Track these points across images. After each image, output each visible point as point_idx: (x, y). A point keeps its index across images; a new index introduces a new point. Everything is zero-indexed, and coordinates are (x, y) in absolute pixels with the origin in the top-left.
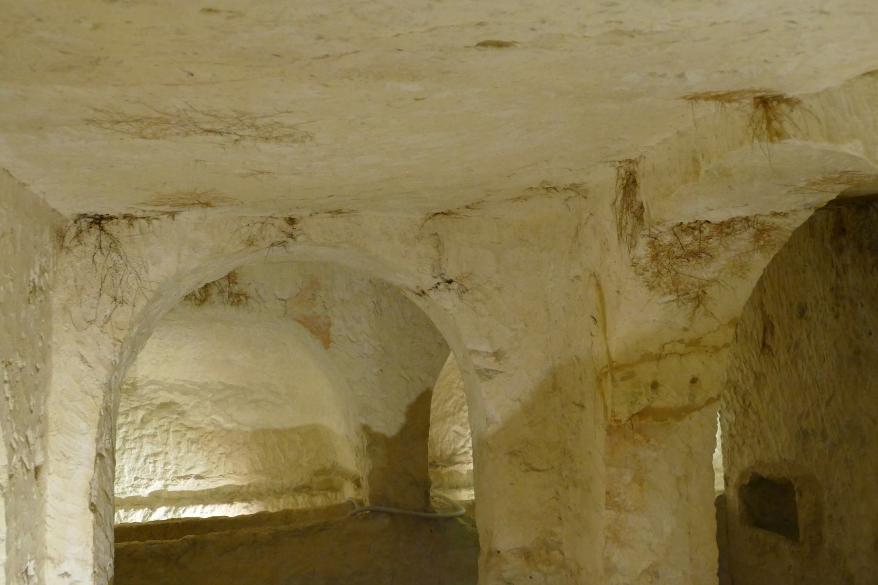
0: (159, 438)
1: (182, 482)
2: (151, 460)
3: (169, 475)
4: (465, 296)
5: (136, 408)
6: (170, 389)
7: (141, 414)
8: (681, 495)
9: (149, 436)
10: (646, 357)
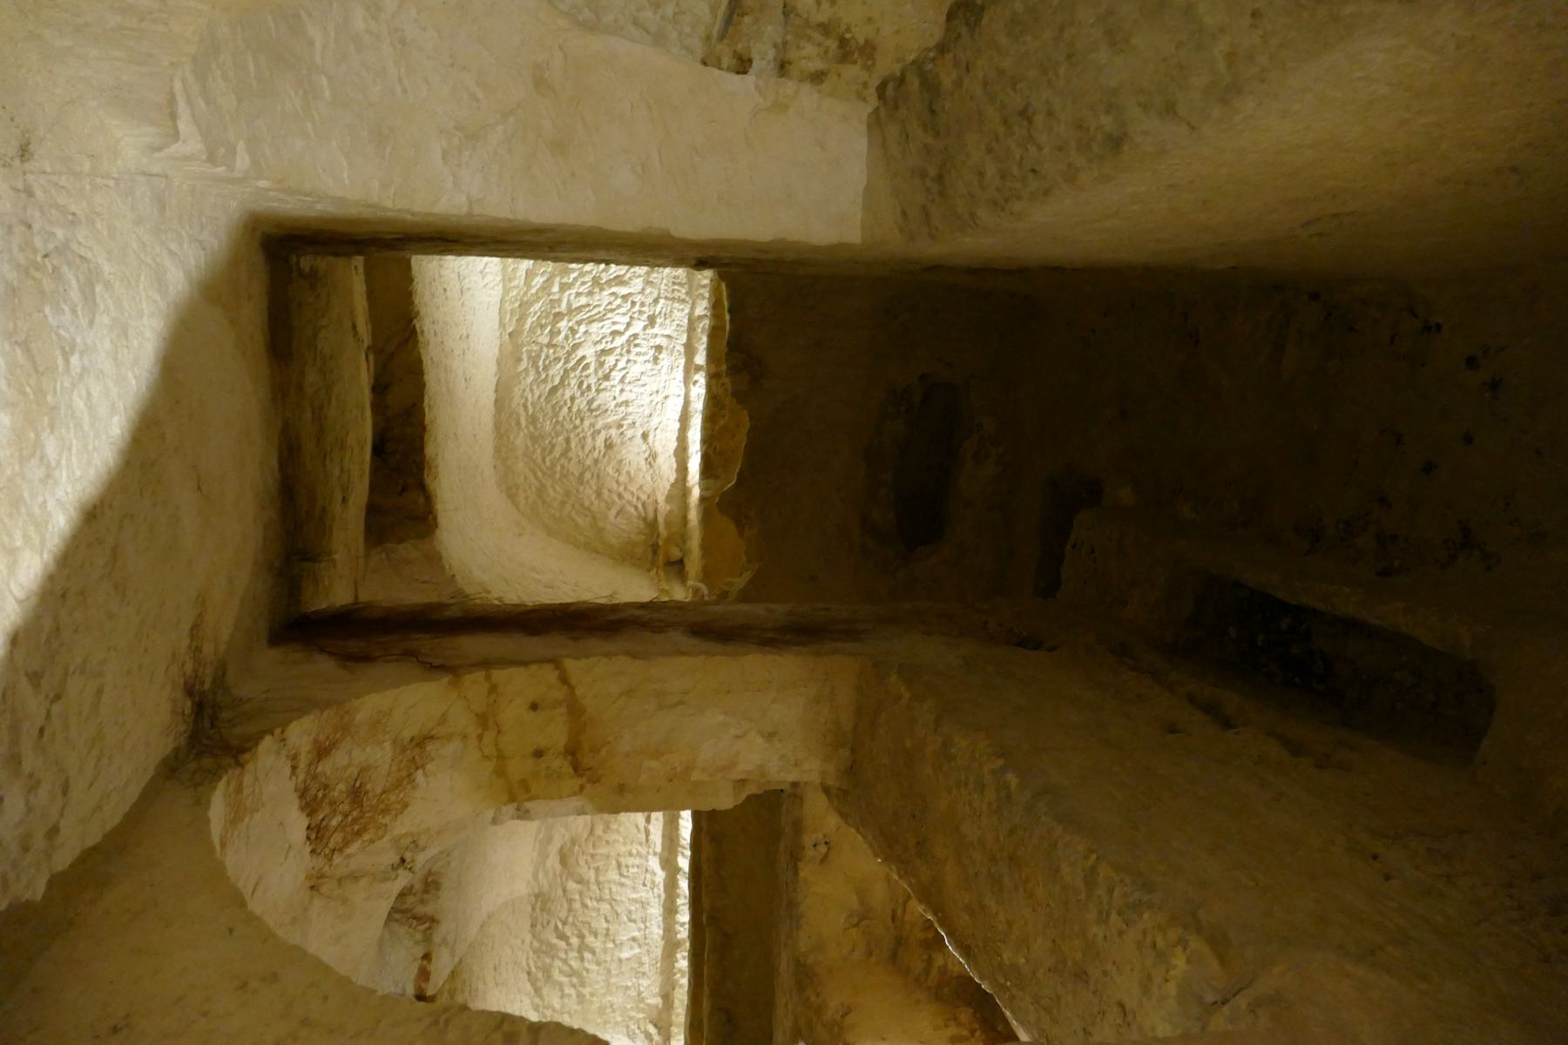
0: (600, 864)
1: (651, 837)
2: (624, 871)
3: (643, 851)
4: (421, 843)
5: (564, 891)
6: (544, 856)
7: (572, 885)
8: (681, 703)
9: (597, 875)
10: (500, 772)
